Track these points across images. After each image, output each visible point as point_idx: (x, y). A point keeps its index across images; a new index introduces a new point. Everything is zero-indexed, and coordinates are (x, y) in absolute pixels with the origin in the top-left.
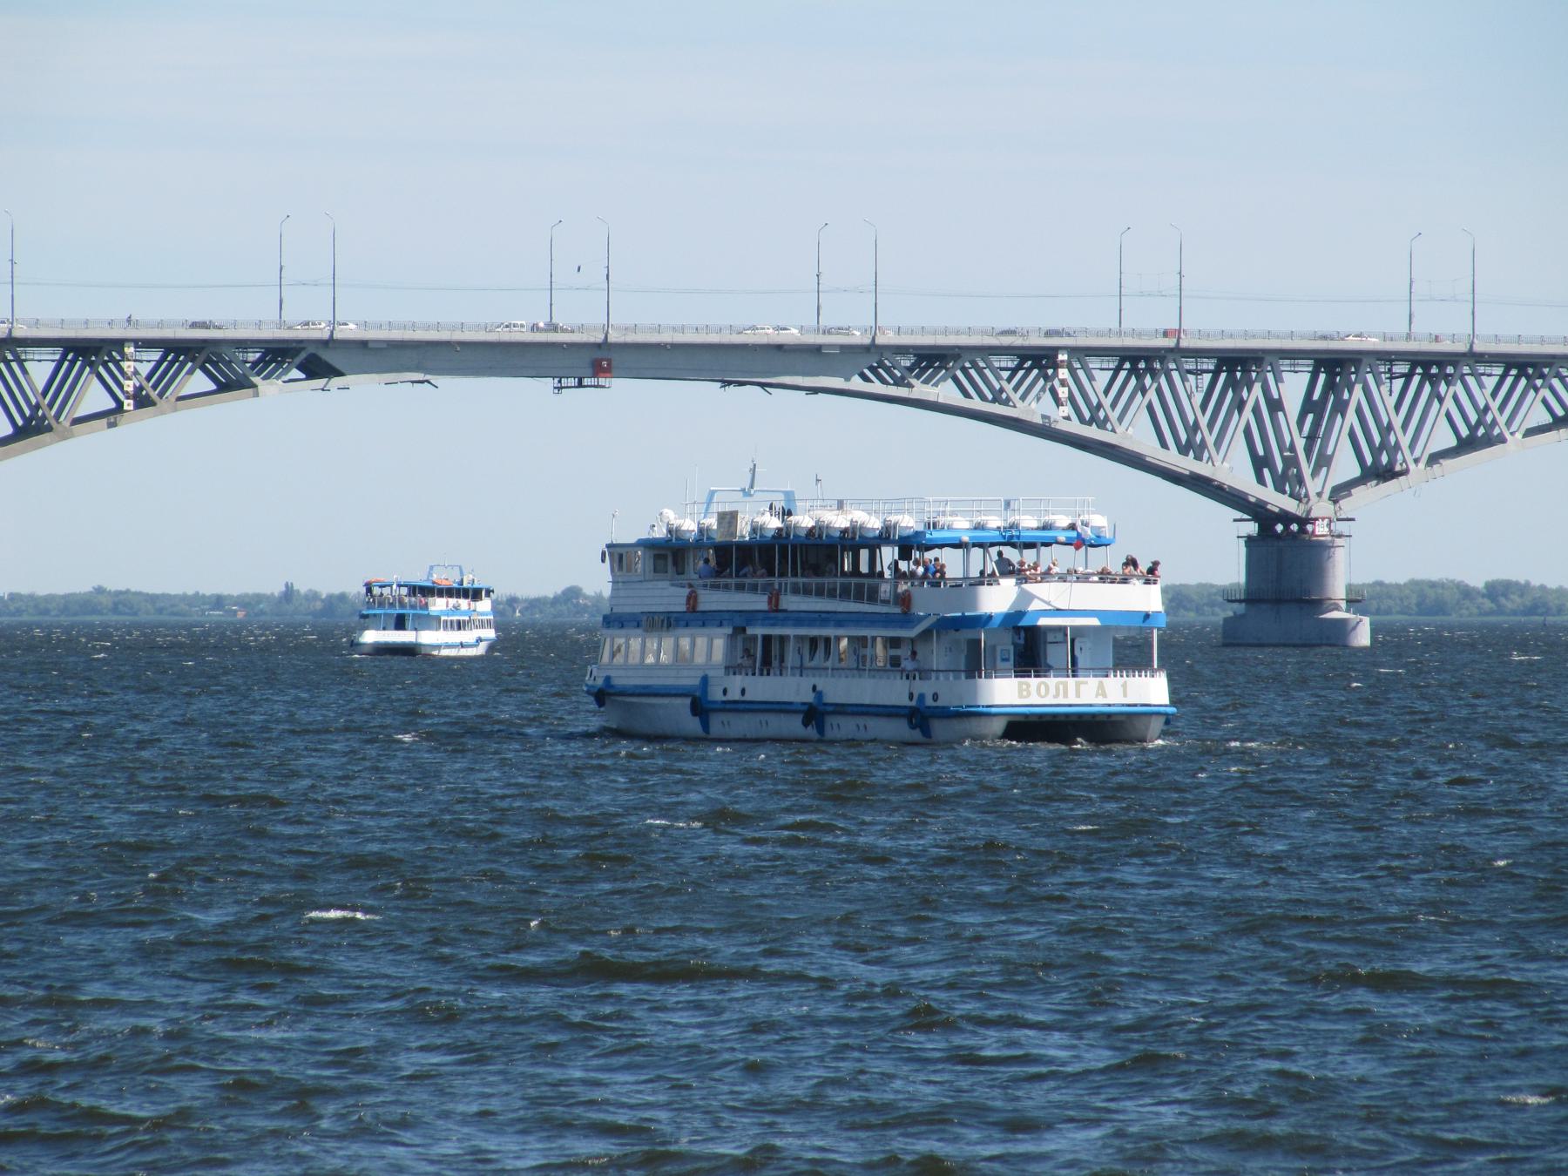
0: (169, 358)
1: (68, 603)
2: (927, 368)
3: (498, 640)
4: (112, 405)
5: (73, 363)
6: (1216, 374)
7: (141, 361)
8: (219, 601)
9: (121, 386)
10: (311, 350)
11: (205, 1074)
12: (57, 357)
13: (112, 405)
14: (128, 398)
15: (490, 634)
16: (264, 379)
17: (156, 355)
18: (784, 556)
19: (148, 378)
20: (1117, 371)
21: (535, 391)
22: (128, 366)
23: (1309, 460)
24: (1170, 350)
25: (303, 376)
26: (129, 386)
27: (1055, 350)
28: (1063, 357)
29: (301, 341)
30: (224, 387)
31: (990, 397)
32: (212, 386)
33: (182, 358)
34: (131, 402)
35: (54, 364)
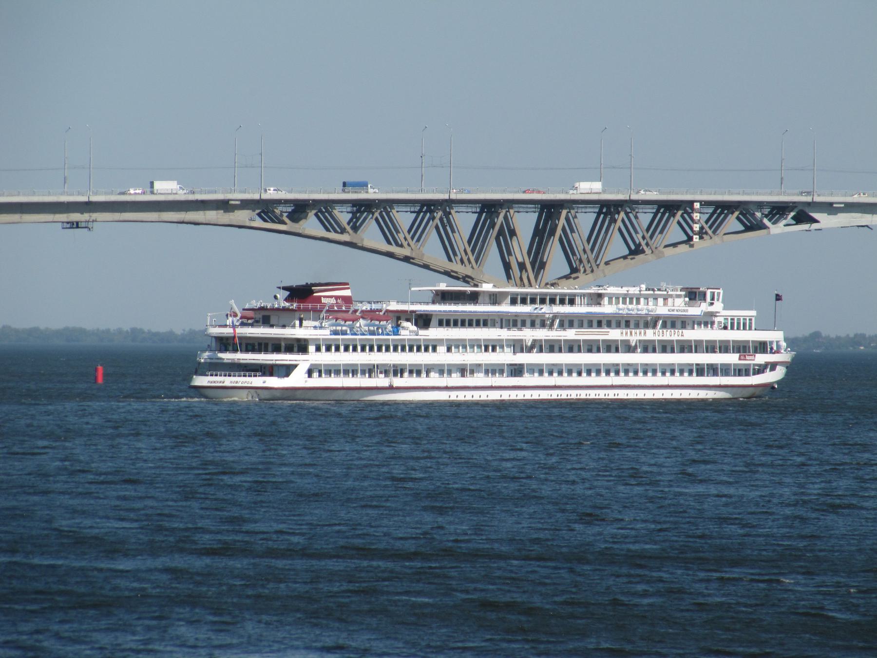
0: (718, 211)
1: (58, 333)
2: (776, 214)
3: (794, 360)
4: (685, 238)
5: (663, 214)
6: (480, 214)
7: (704, 213)
8: (170, 336)
9: (691, 228)
10: (800, 208)
11: (870, 508)
12: (597, 210)
13: (685, 238)
14: (696, 234)
15: (785, 356)
16: (773, 223)
17: (710, 210)
18: (745, 325)
19: (707, 222)
20: (599, 214)
21: (193, 225)
22: (696, 216)
23: (533, 271)
24: (446, 201)
25: (794, 222)
26: (696, 227)
27: (691, 203)
28: (697, 205)
29: (794, 203)
30: (749, 228)
31: (339, 231)
32: (742, 228)
33: (726, 212)
34: (698, 237)
35: (653, 215)
